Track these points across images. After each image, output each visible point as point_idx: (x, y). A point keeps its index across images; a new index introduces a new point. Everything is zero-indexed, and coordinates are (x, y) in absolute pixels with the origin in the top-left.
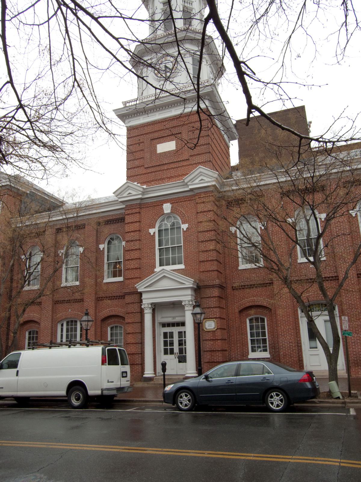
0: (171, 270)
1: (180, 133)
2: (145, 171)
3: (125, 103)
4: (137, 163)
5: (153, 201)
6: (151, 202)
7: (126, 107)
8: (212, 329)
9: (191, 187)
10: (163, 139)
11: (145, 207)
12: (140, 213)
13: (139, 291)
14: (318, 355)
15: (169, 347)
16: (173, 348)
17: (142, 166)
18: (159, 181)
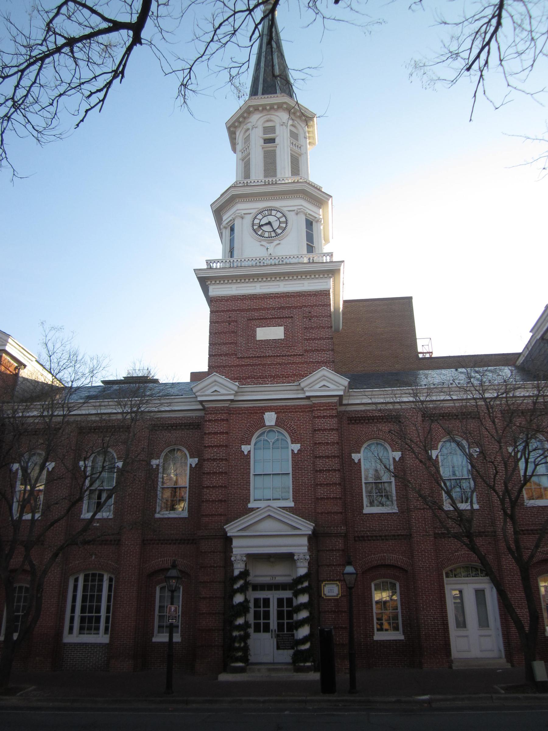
0: (280, 507)
1: (292, 317)
2: (237, 362)
3: (208, 262)
4: (225, 349)
8: (334, 596)
9: (308, 394)
10: (267, 321)
12: (227, 420)
13: (229, 534)
14: (467, 636)
15: (262, 621)
16: (269, 623)
17: (232, 354)
18: (258, 378)
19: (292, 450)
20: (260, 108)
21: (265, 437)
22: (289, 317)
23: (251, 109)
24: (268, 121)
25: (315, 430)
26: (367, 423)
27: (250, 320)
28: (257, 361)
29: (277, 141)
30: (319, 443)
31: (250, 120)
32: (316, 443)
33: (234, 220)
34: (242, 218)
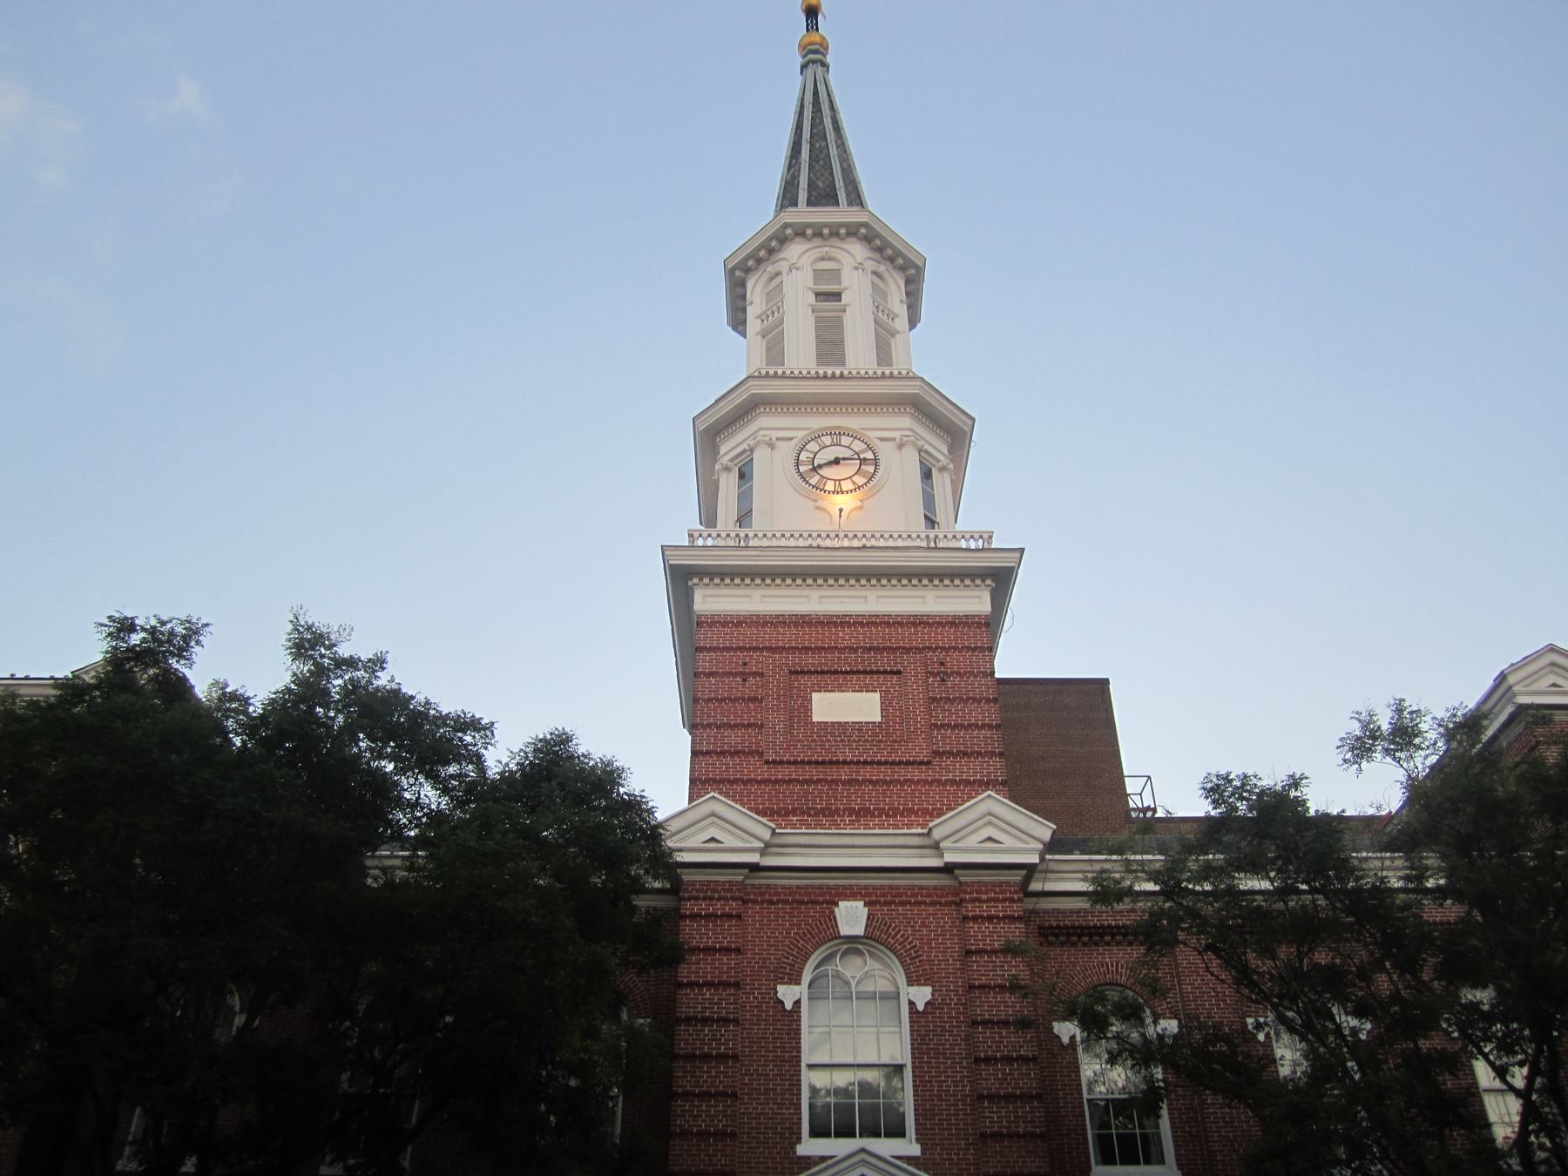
1: (899, 672)
2: (764, 772)
4: (734, 739)
5: (798, 882)
6: (784, 887)
7: (692, 547)
9: (950, 858)
11: (763, 902)
17: (751, 753)
18: (817, 815)
19: (911, 1003)
20: (809, 232)
21: (838, 965)
22: (892, 672)
23: (789, 231)
24: (823, 259)
25: (969, 953)
26: (1085, 944)
27: (796, 672)
28: (815, 773)
29: (843, 297)
30: (981, 987)
31: (783, 255)
32: (972, 987)
33: (752, 450)
34: (772, 446)
